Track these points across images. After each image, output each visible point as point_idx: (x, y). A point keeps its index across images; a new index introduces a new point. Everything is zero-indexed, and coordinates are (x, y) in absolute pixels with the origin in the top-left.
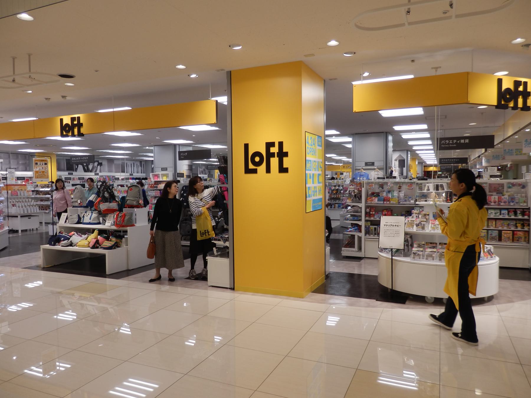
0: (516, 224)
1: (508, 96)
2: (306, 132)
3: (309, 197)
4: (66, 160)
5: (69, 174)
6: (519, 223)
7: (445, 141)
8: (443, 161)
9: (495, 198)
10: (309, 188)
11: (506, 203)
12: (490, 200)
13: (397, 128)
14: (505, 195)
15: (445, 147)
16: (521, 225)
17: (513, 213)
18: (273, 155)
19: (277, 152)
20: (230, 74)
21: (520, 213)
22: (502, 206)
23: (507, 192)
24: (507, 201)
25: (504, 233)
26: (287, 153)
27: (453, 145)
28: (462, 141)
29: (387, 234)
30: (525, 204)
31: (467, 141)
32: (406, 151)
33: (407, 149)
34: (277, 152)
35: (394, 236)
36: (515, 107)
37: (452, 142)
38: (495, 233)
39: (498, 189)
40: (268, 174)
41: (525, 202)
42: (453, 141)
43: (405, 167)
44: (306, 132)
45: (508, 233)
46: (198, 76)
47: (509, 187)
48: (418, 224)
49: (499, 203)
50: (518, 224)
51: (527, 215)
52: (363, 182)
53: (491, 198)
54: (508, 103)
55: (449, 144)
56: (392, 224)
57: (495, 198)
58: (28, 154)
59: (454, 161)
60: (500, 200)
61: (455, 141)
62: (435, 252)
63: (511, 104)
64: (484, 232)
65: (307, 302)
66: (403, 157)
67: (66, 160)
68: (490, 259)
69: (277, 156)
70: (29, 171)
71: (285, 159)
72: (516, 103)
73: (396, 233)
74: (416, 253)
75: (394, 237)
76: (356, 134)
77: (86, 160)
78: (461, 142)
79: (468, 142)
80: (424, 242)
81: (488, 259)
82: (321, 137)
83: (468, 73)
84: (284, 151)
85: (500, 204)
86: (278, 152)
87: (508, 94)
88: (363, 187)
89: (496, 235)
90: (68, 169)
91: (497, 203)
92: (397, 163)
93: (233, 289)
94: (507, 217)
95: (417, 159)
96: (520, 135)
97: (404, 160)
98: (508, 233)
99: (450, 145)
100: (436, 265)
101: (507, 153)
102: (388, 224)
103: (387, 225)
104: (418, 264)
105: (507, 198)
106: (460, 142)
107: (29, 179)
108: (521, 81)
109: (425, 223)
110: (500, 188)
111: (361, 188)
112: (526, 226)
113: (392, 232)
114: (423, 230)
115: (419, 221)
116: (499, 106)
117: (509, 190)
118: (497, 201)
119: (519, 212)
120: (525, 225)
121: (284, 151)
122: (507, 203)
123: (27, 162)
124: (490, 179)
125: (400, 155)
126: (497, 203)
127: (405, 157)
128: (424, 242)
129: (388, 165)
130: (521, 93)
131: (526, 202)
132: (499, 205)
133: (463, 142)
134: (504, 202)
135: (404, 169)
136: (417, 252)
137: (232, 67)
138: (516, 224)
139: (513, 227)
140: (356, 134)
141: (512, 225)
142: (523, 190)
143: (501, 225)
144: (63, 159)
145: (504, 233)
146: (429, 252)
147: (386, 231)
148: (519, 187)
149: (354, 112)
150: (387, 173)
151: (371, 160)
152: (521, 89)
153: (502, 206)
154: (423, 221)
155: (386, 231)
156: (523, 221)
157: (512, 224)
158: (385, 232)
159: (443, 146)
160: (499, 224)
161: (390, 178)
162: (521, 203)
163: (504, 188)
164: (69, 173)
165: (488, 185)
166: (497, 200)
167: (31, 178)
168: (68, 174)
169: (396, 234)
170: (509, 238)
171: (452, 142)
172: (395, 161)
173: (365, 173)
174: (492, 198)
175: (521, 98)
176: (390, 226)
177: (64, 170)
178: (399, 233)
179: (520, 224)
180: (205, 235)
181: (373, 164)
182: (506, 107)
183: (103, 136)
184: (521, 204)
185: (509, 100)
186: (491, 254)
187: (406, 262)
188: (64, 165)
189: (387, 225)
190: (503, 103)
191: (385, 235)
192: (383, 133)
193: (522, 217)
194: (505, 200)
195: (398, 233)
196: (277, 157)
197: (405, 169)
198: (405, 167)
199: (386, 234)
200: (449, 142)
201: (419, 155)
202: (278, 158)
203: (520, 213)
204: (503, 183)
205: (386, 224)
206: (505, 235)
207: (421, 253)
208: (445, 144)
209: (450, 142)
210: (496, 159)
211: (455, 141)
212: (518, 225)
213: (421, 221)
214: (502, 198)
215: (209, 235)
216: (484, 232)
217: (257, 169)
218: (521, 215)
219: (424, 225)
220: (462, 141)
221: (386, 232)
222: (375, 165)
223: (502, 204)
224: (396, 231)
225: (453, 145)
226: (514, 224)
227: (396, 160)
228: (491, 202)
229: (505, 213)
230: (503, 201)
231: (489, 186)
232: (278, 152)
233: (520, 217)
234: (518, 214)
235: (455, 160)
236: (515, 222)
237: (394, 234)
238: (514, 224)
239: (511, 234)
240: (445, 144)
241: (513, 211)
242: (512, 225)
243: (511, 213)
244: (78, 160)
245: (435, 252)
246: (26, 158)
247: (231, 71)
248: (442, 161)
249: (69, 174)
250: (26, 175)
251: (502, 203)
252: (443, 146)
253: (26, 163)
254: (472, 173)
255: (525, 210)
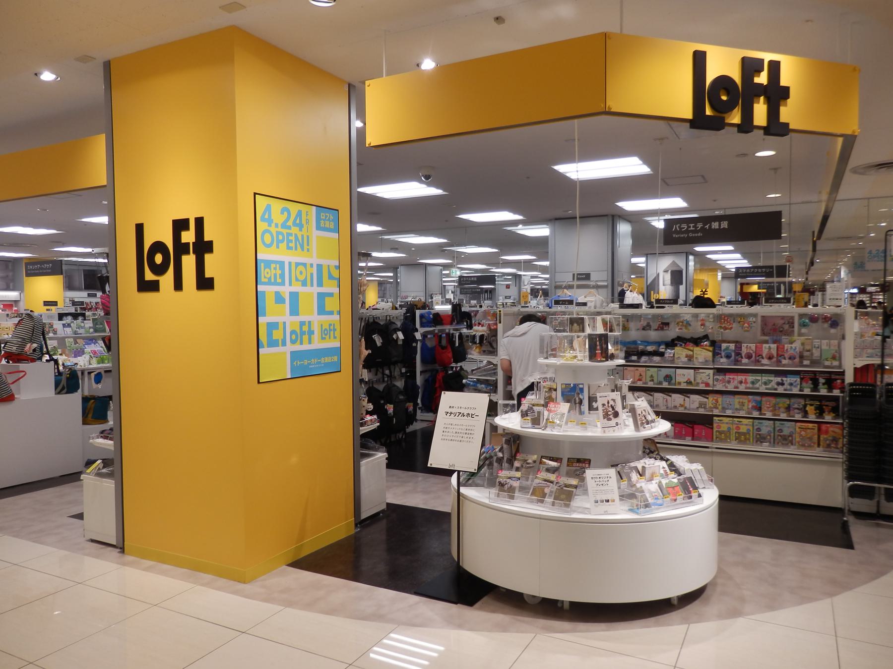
0: (805, 406)
1: (724, 98)
2: (255, 194)
3: (273, 343)
4: (84, 271)
5: (89, 295)
6: (811, 405)
7: (681, 225)
8: (743, 273)
9: (770, 348)
10: (272, 326)
11: (796, 360)
12: (760, 353)
13: (629, 205)
14: (795, 341)
15: (679, 238)
16: (815, 410)
17: (810, 382)
18: (331, 330)
19: (193, 243)
20: (107, 65)
21: (824, 384)
22: (784, 366)
23: (800, 335)
24: (796, 354)
25: (799, 428)
26: (210, 243)
27: (696, 235)
28: (715, 225)
29: (449, 434)
30: (836, 363)
31: (725, 225)
32: (685, 254)
33: (688, 251)
34: (193, 243)
35: (461, 439)
36: (746, 126)
37: (693, 227)
38: (767, 426)
39: (781, 329)
40: (179, 293)
41: (834, 358)
42: (696, 225)
43: (682, 284)
44: (255, 194)
45: (809, 429)
46: (59, 79)
47: (804, 325)
48: (527, 411)
49: (780, 358)
50: (808, 406)
51: (840, 389)
52: (500, 311)
53: (762, 348)
54: (725, 115)
55: (687, 231)
56: (462, 411)
57: (770, 348)
58: (12, 260)
59: (762, 272)
60: (780, 353)
61: (700, 225)
62: (552, 482)
63: (735, 118)
64: (746, 425)
65: (240, 597)
66: (679, 266)
67: (84, 271)
68: (684, 501)
69: (194, 252)
70: (13, 290)
71: (208, 257)
72: (748, 115)
73: (467, 432)
74: (506, 484)
75: (461, 441)
76: (556, 219)
77: (49, 269)
78: (713, 227)
79: (726, 227)
80: (536, 456)
81: (678, 502)
82: (338, 210)
83: (605, 36)
84: (206, 239)
85: (781, 362)
86: (194, 241)
87: (722, 92)
88: (500, 322)
89: (769, 431)
90: (87, 287)
91: (775, 359)
92: (668, 277)
93: (121, 548)
94: (795, 391)
95: (719, 271)
96: (888, 220)
97: (681, 272)
98: (809, 429)
99: (691, 235)
100: (540, 518)
101: (874, 257)
102: (453, 410)
103: (451, 413)
104: (497, 510)
105: (796, 348)
106: (710, 227)
107: (13, 303)
108: (763, 60)
109: (541, 408)
110: (786, 327)
111: (496, 324)
112: (826, 413)
113: (458, 431)
114: (536, 426)
115: (527, 405)
116: (698, 121)
117: (804, 330)
118: (775, 355)
119: (822, 381)
120: (826, 410)
121: (206, 239)
122: (797, 360)
123: (11, 274)
124: (108, 293)
125: (673, 261)
126: (775, 359)
127: (683, 266)
128: (536, 456)
129: (617, 279)
130: (761, 90)
131: (837, 358)
132: (757, 362)
133: (717, 227)
134: (790, 358)
135: (681, 287)
136: (508, 480)
137: (111, 54)
138: (805, 406)
139: (798, 413)
140: (556, 219)
141: (798, 409)
142: (833, 331)
143: (771, 409)
144: (78, 270)
145: (799, 428)
146: (541, 482)
147: (446, 428)
148: (826, 325)
149: (367, 146)
150: (614, 296)
151: (583, 270)
152: (762, 79)
153: (784, 366)
154: (538, 405)
155: (446, 428)
156: (820, 401)
157: (796, 406)
158: (445, 430)
159: (677, 236)
160: (768, 406)
161: (562, 304)
162: (827, 360)
163: (793, 327)
164: (88, 294)
165: (759, 319)
166: (774, 352)
167: (16, 302)
168: (87, 296)
169: (467, 435)
170: (810, 439)
171: (693, 227)
172: (665, 273)
173: (570, 296)
174: (764, 349)
175: (764, 104)
176: (458, 414)
177: (79, 289)
178: (472, 432)
179: (813, 407)
180: (169, 276)
181: (587, 276)
182: (717, 124)
183: (85, 225)
184: (827, 363)
185: (728, 107)
186: (691, 489)
187: (474, 502)
188: (80, 280)
189: (451, 413)
190: (708, 112)
191: (443, 437)
192: (605, 218)
193: (828, 392)
194: (792, 352)
195: (470, 432)
196: (193, 253)
197: (682, 288)
198: (682, 284)
199: (446, 434)
200: (687, 228)
201: (718, 262)
202: (195, 256)
203: (824, 384)
204: (791, 315)
205: (450, 410)
206: (803, 433)
207: (516, 484)
208: (681, 232)
209: (690, 227)
210: (860, 269)
211: (700, 225)
212: (808, 408)
213: (534, 405)
214: (786, 349)
215: (205, 283)
216: (747, 423)
217: (158, 281)
218: (826, 386)
219: (539, 413)
220: (715, 225)
221: (447, 430)
222: (592, 279)
223: (784, 362)
224: (468, 428)
225: (696, 235)
226: (801, 406)
227: (666, 271)
228: (763, 358)
229: (796, 381)
230: (786, 355)
231: (762, 321)
232: (194, 241)
233: (823, 392)
234: (821, 384)
235: (764, 270)
236: (802, 402)
237: (461, 435)
238: (801, 406)
239: (816, 431)
240: (681, 232)
241: (811, 379)
242: (798, 409)
243: (807, 383)
244: (37, 269)
245: (552, 482)
246: (7, 267)
247: (110, 61)
248: (740, 273)
249: (89, 295)
250: (6, 296)
251: (785, 359)
252: (677, 236)
253: (7, 276)
254: (620, 291)
255: (833, 377)
